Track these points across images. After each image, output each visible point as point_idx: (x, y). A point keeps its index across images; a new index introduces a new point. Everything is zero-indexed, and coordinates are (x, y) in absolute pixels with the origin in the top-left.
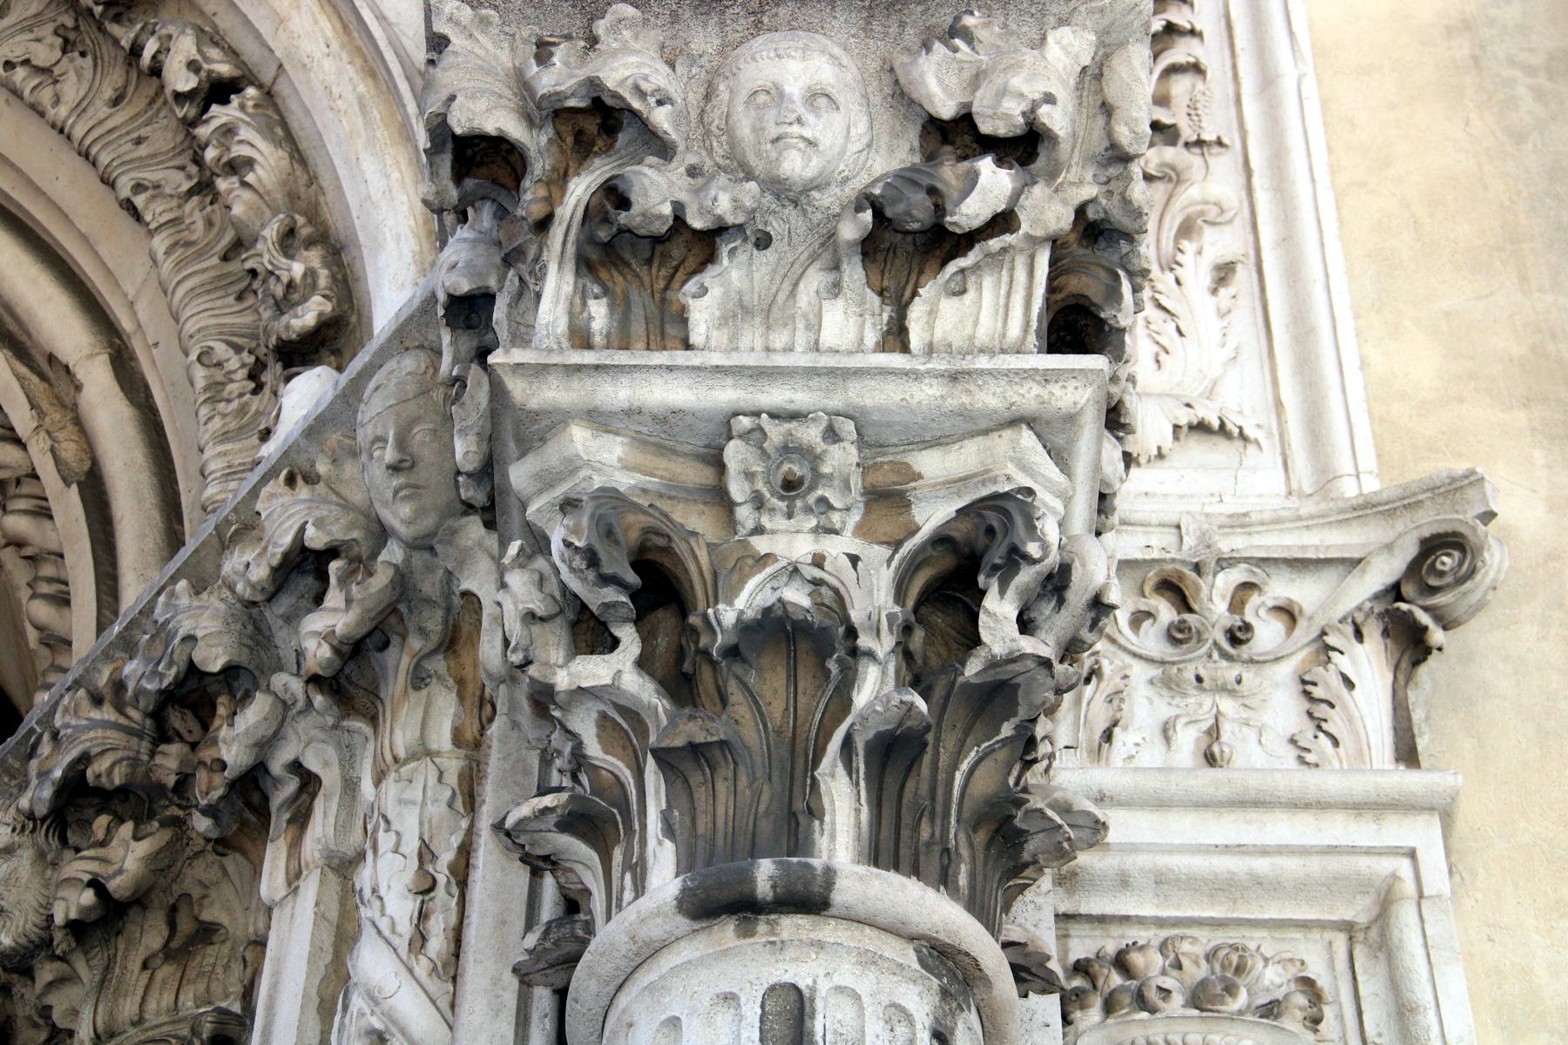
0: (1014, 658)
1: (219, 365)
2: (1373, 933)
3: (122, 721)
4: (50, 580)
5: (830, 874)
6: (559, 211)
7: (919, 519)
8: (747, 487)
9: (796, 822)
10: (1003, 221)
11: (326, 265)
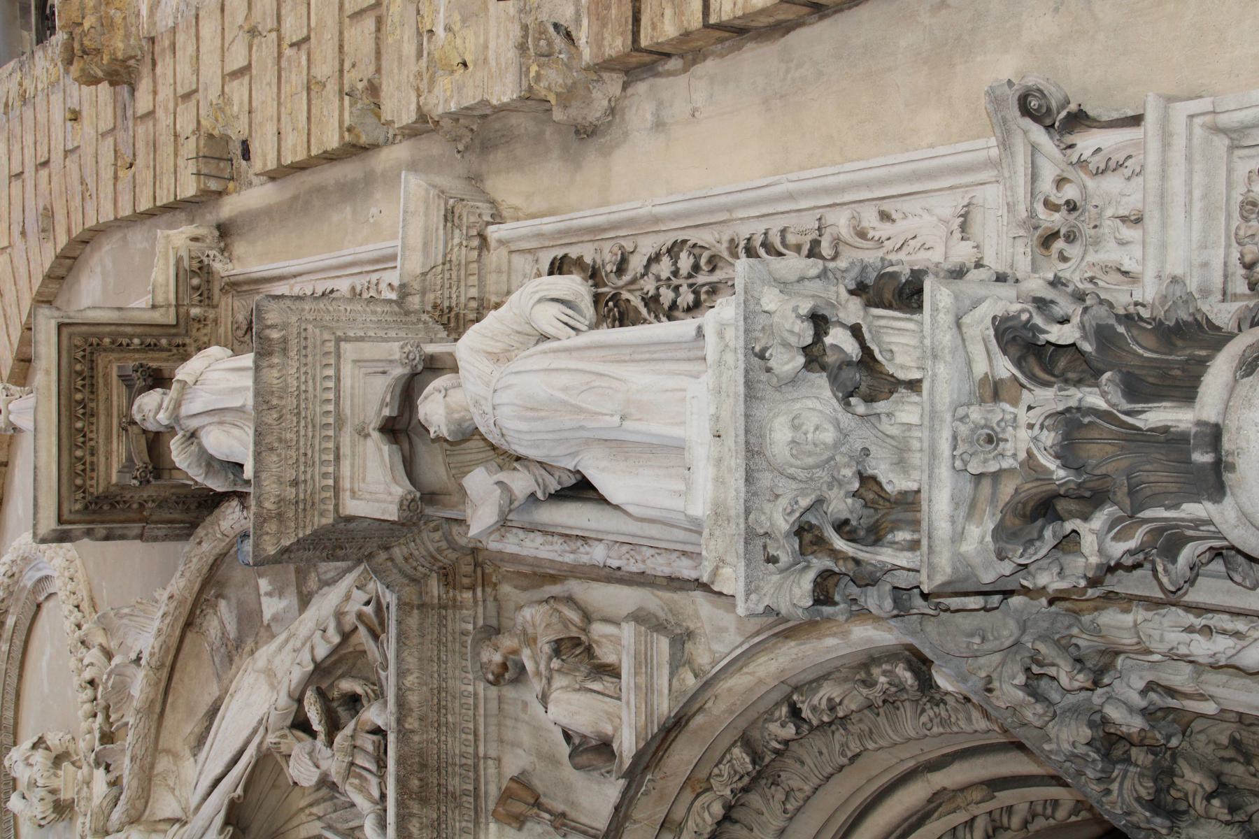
0: (1082, 327)
1: (931, 720)
2: (1234, 136)
3: (1119, 780)
4: (1045, 808)
5: (1199, 423)
6: (851, 554)
7: (1009, 374)
8: (991, 462)
9: (1171, 442)
10: (856, 331)
11: (880, 665)
